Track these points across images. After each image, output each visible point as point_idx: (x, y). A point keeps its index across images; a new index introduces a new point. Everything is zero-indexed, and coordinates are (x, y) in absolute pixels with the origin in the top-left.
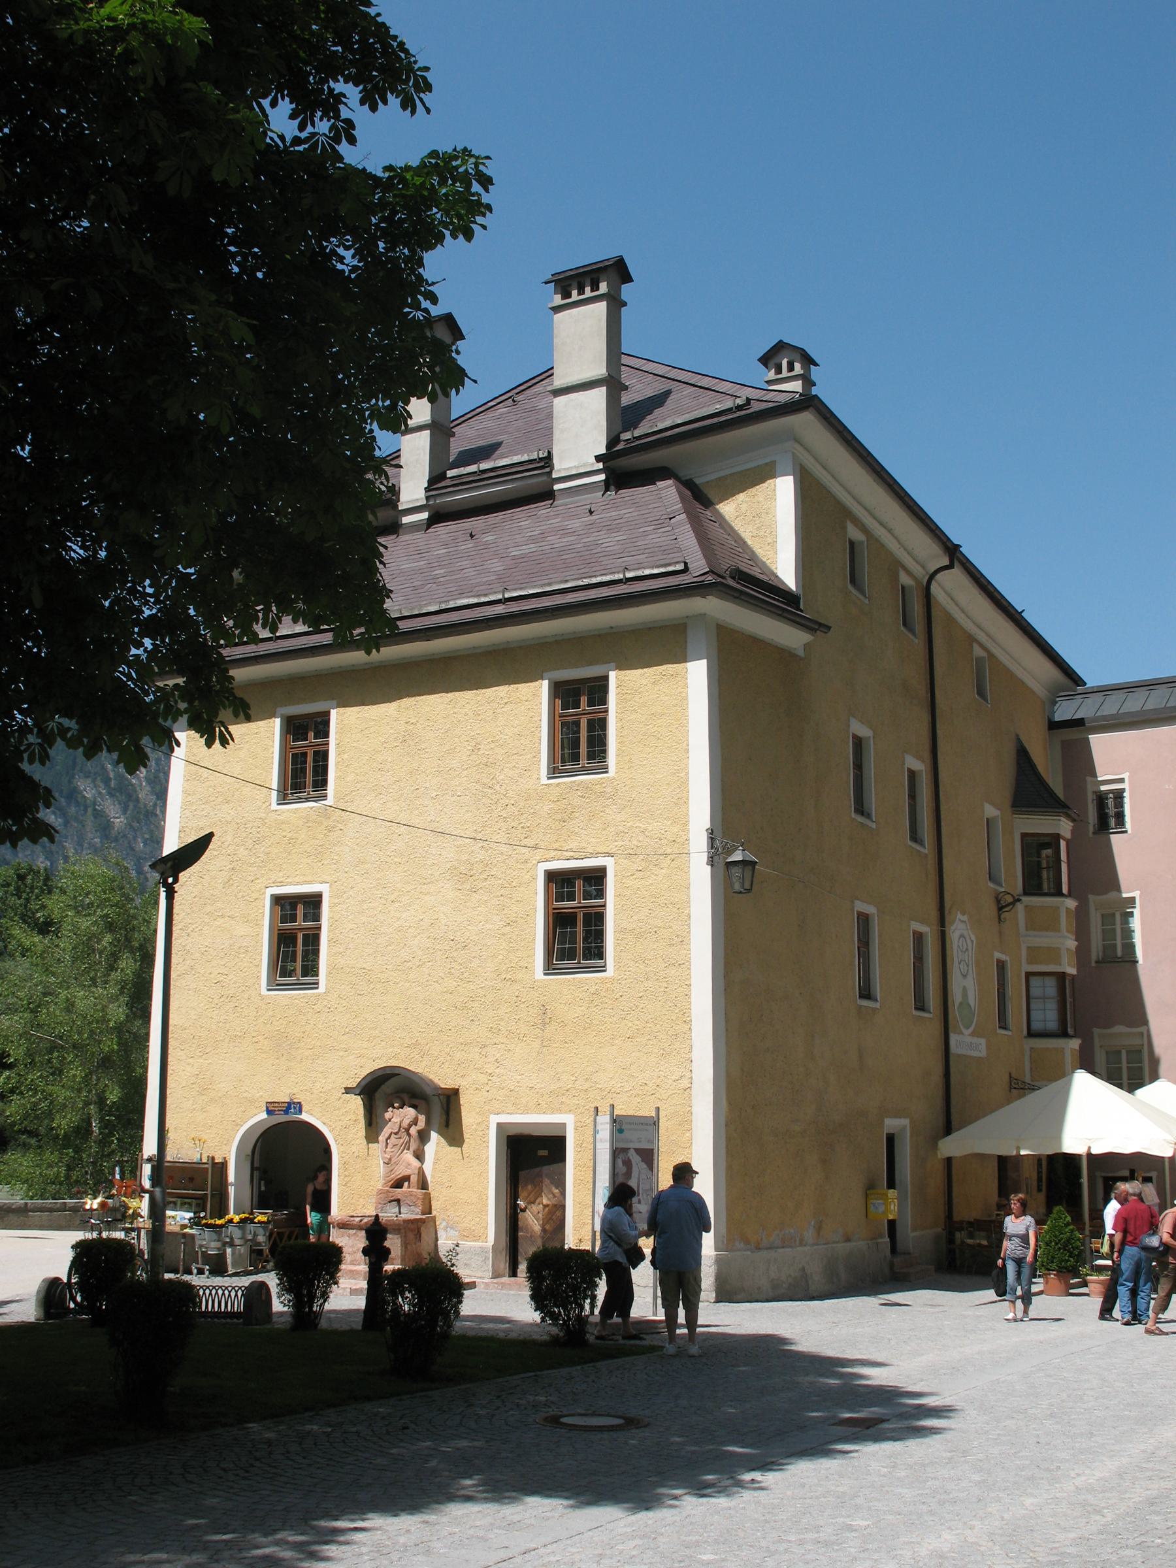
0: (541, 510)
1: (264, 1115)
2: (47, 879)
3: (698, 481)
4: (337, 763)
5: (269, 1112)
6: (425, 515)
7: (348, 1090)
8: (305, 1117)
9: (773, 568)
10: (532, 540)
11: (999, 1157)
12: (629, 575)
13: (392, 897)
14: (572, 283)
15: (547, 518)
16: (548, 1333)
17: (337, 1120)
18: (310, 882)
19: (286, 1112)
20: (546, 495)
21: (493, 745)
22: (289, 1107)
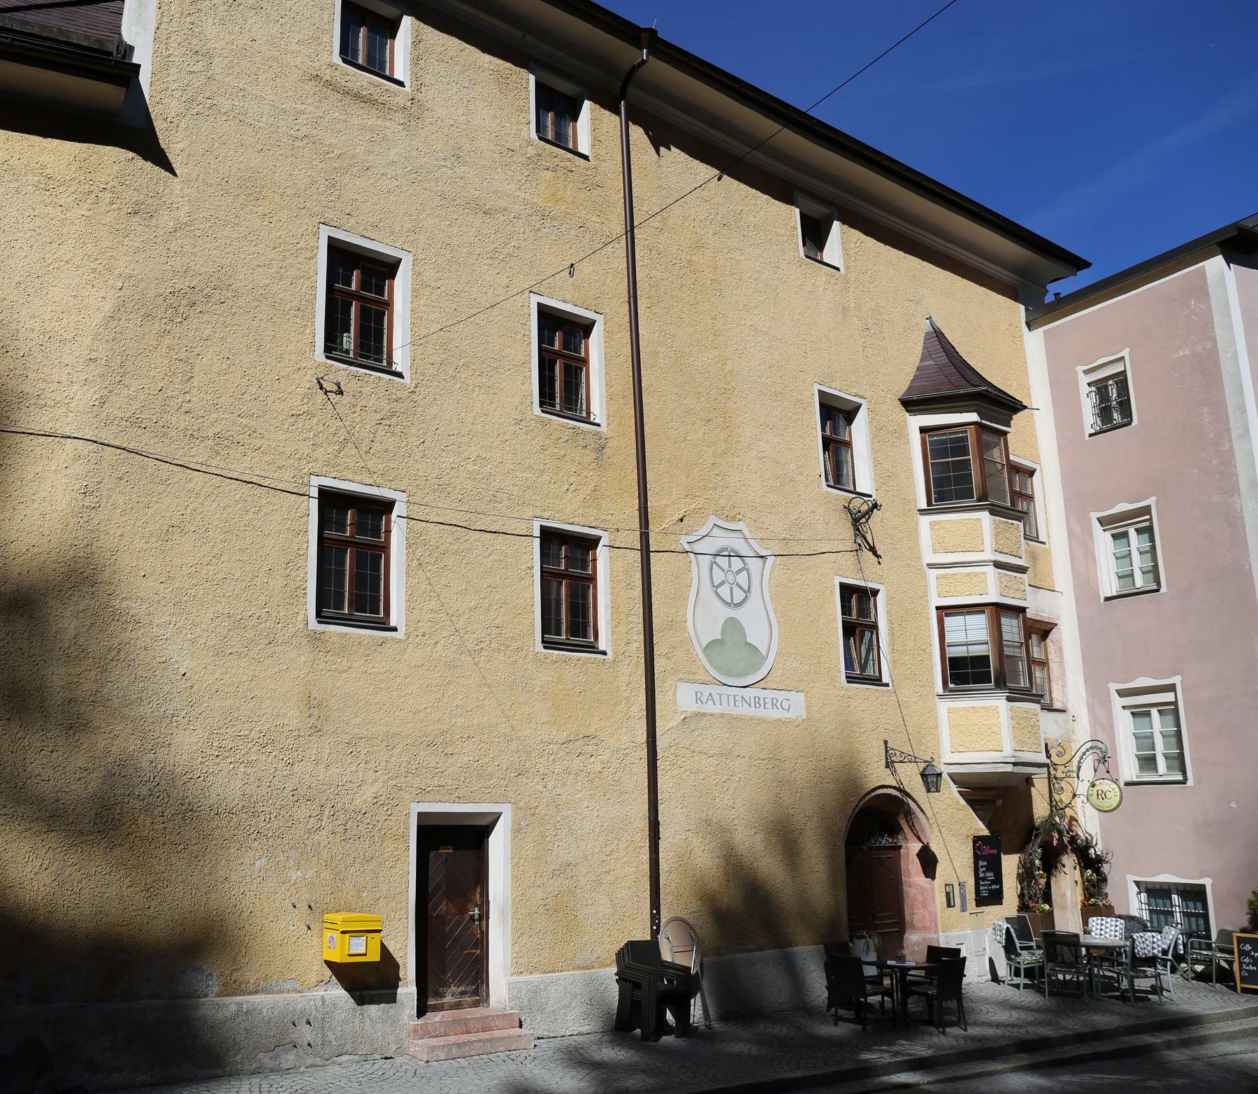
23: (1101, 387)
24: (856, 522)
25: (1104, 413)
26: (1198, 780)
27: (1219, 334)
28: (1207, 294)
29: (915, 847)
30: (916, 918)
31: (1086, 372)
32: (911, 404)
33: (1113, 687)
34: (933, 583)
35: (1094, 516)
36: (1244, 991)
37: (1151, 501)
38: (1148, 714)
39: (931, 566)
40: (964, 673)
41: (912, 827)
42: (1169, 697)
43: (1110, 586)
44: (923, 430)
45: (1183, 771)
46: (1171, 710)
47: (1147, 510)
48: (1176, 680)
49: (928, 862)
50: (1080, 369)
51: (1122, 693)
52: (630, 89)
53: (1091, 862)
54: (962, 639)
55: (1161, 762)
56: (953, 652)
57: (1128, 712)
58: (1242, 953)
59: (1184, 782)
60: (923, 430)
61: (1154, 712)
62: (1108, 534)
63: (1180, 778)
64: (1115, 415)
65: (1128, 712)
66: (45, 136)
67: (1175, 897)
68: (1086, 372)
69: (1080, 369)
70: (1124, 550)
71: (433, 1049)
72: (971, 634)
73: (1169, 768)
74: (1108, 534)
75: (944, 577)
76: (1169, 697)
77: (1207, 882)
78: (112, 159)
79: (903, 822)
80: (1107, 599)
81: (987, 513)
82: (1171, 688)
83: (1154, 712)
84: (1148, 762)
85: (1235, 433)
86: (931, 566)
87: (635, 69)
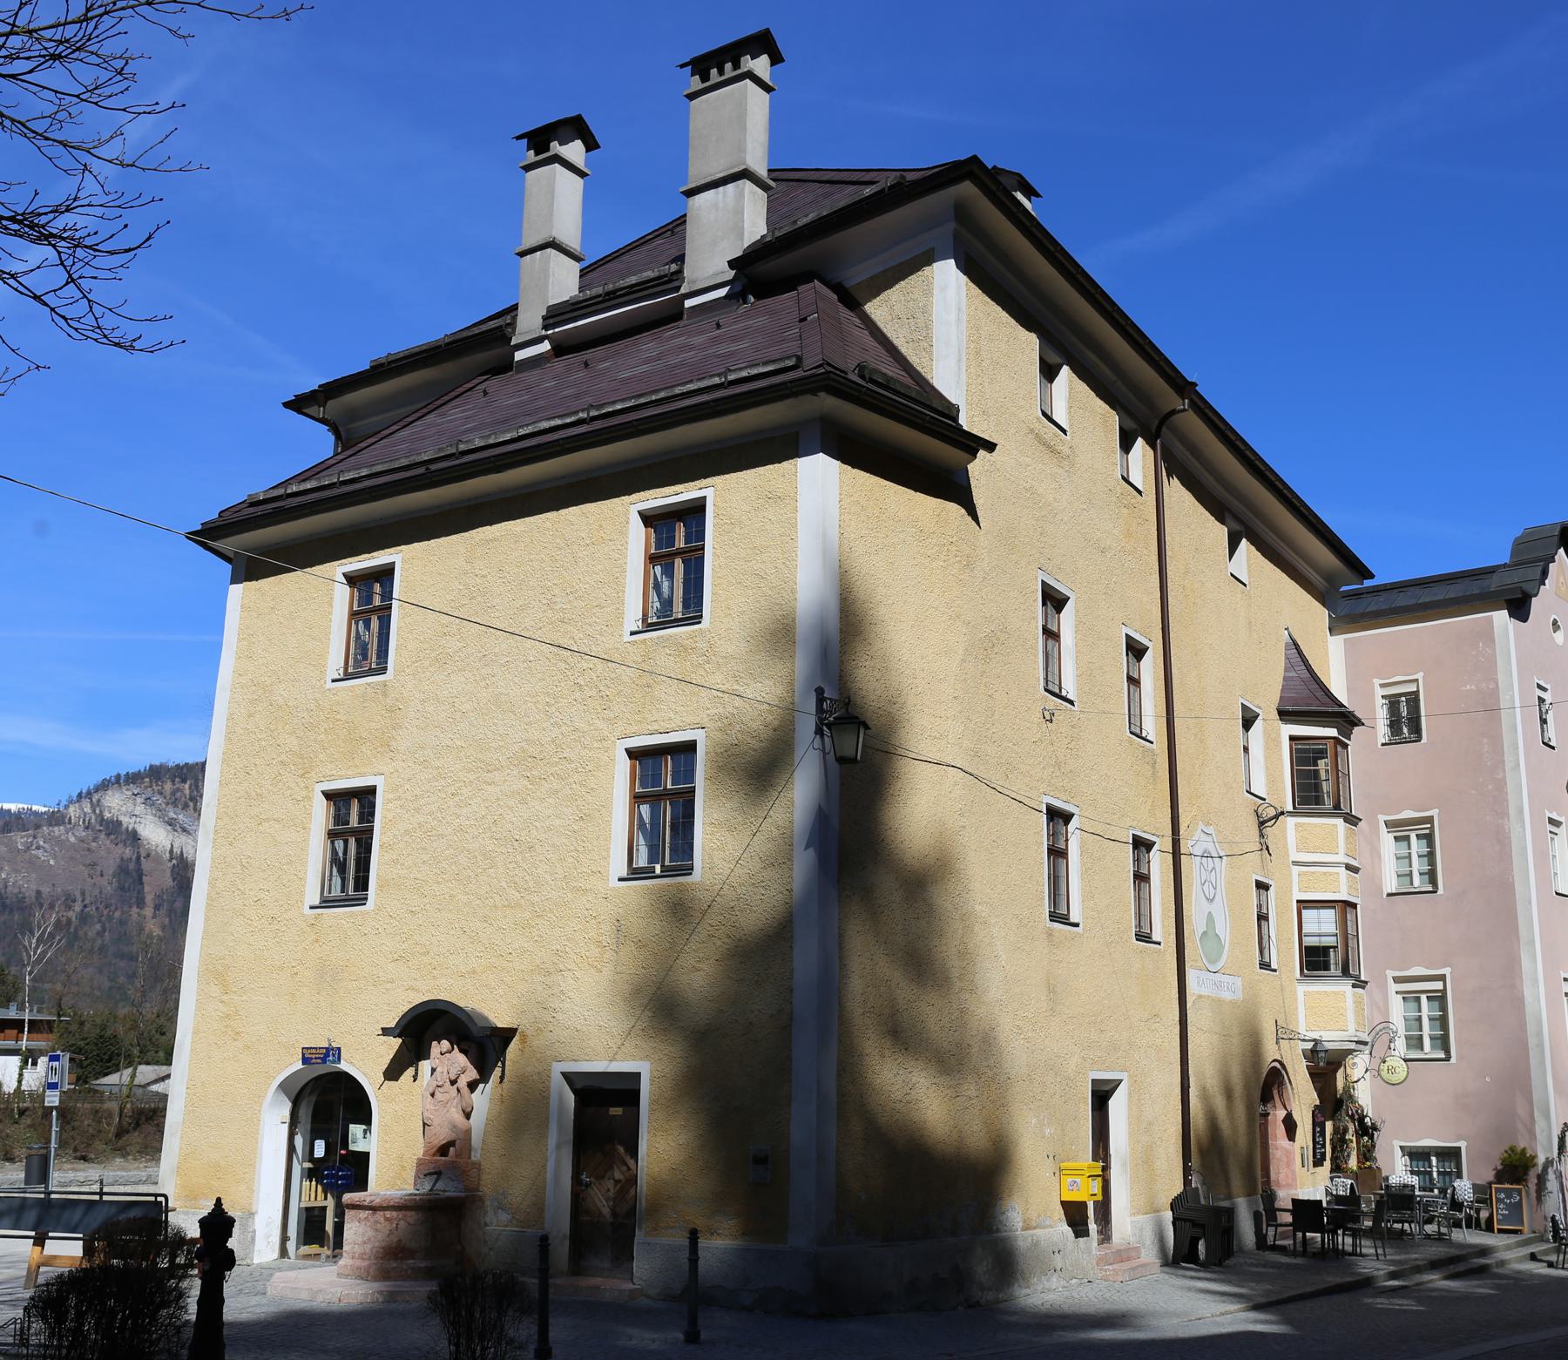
0: (668, 332)
1: (299, 1065)
2: (184, 830)
3: (849, 284)
4: (399, 628)
5: (305, 1060)
6: (546, 346)
7: (386, 1032)
8: (344, 1066)
9: (928, 377)
10: (648, 361)
11: (204, 764)
12: (731, 377)
13: (452, 789)
14: (715, 65)
15: (673, 337)
16: (381, 1292)
17: (366, 1061)
18: (363, 775)
19: (324, 1060)
20: (673, 315)
21: (571, 597)
22: (327, 1055)
23: (1393, 703)
24: (1262, 824)
25: (1395, 725)
26: (1460, 1058)
27: (1501, 678)
28: (1493, 641)
29: (1282, 1114)
30: (1281, 1176)
31: (1382, 686)
32: (1285, 715)
33: (1390, 974)
34: (1295, 878)
35: (1382, 818)
36: (1500, 1231)
37: (1434, 812)
38: (1418, 1000)
39: (1295, 863)
40: (1315, 960)
41: (1281, 1096)
42: (1439, 985)
43: (1391, 884)
44: (1292, 738)
45: (1447, 1051)
46: (1440, 999)
47: (1430, 820)
48: (1447, 971)
49: (1290, 1126)
50: (1377, 682)
51: (1397, 980)
52: (1164, 429)
53: (1366, 1130)
54: (1316, 931)
55: (1427, 1042)
56: (1308, 941)
57: (1400, 997)
58: (1498, 1200)
59: (1448, 1059)
60: (1292, 738)
61: (1424, 997)
62: (1391, 836)
63: (1442, 1056)
64: (1405, 730)
65: (1400, 997)
66: (916, 490)
67: (1434, 1159)
68: (1382, 686)
69: (1377, 682)
70: (1405, 852)
71: (1116, 1272)
72: (1322, 925)
73: (1433, 1047)
74: (1391, 836)
75: (1305, 873)
76: (1439, 985)
77: (1462, 1144)
78: (954, 510)
79: (1275, 1092)
80: (1389, 895)
81: (1341, 820)
82: (1442, 978)
83: (1424, 997)
84: (1415, 1042)
85: (1508, 765)
86: (1295, 863)
87: (1174, 412)
